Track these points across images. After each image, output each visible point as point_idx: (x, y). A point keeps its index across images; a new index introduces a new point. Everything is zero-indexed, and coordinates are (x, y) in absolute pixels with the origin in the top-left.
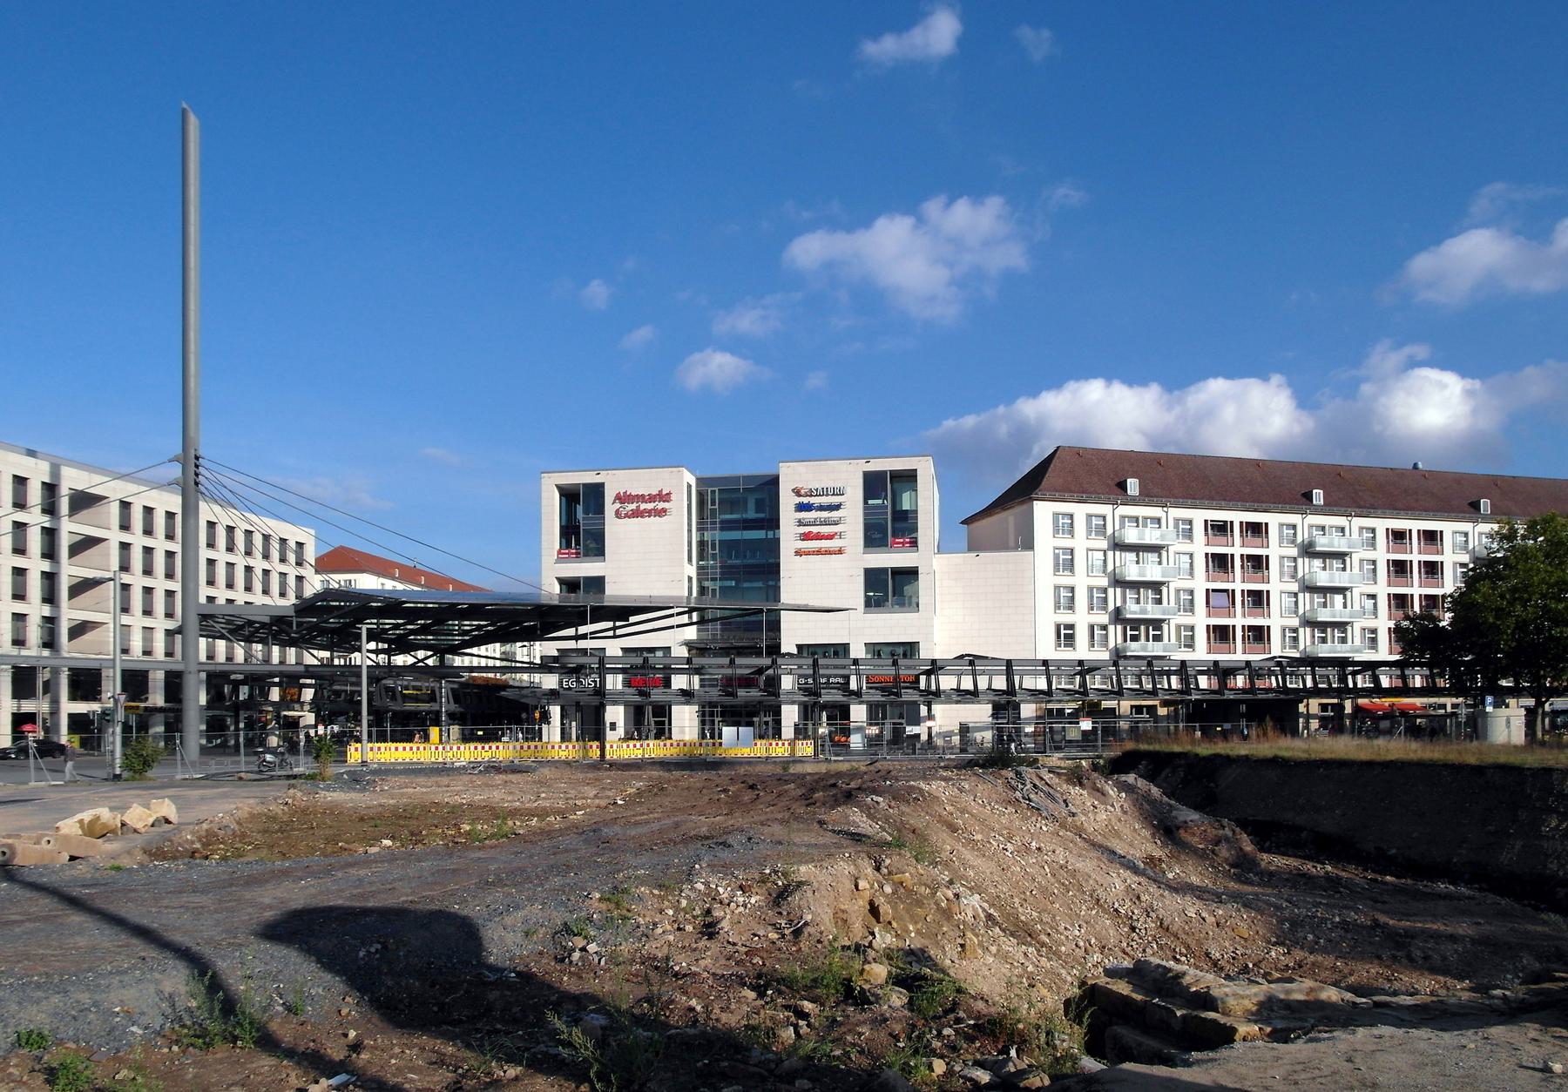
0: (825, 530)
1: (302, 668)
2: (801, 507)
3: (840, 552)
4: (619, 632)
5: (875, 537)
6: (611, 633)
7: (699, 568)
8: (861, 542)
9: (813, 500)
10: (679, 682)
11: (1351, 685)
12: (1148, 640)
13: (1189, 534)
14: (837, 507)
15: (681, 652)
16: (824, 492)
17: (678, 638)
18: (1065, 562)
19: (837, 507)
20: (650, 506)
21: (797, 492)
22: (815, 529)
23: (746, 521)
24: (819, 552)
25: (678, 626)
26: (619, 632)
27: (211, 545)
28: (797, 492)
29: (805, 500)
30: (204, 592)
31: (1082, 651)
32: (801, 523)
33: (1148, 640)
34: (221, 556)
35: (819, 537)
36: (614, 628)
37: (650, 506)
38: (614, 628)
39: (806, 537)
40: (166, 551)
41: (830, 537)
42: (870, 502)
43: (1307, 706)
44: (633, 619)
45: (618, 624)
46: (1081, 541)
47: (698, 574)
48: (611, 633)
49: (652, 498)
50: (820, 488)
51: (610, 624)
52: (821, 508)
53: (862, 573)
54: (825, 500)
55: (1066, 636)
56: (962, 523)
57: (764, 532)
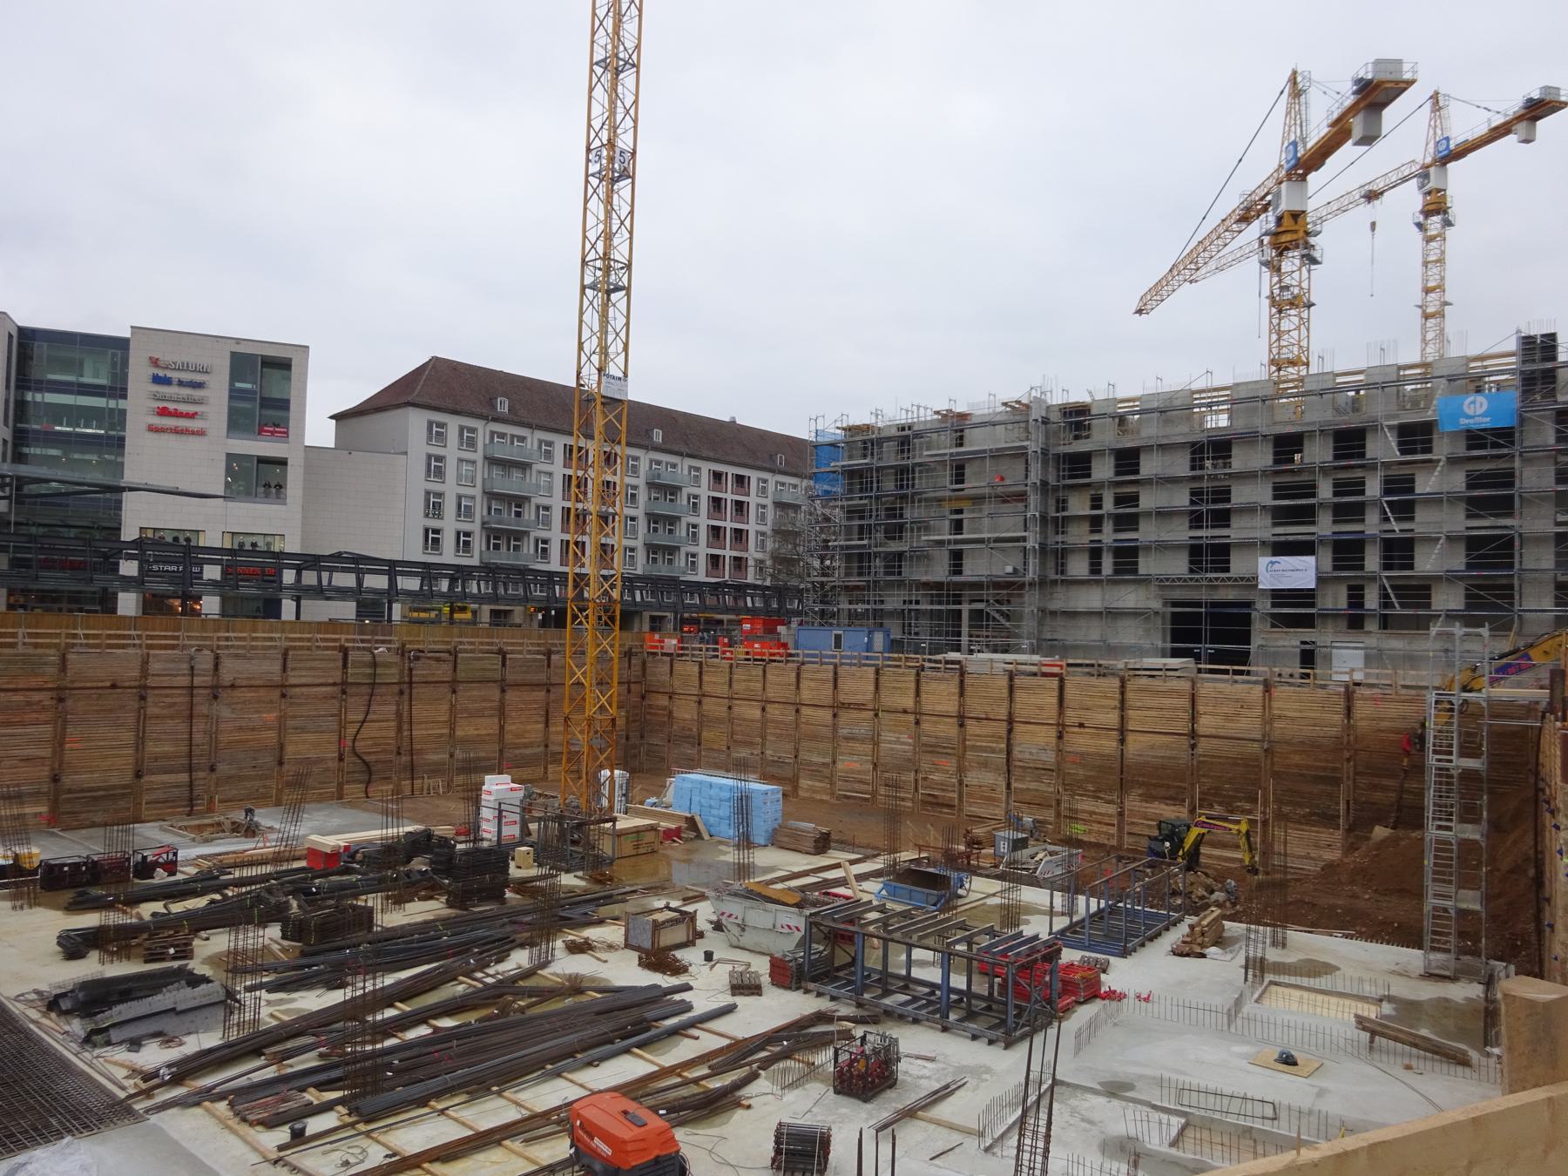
0: (183, 408)
2: (157, 380)
3: (201, 433)
5: (237, 423)
9: (175, 375)
11: (750, 604)
12: (509, 549)
13: (549, 455)
16: (184, 367)
18: (435, 467)
19: (199, 385)
22: (171, 406)
23: (81, 385)
24: (177, 431)
28: (155, 362)
29: (161, 373)
31: (448, 555)
32: (156, 398)
33: (509, 549)
39: (163, 412)
41: (192, 416)
42: (238, 385)
46: (452, 451)
47: (15, 438)
52: (181, 383)
54: (186, 376)
55: (432, 539)
56: (331, 417)
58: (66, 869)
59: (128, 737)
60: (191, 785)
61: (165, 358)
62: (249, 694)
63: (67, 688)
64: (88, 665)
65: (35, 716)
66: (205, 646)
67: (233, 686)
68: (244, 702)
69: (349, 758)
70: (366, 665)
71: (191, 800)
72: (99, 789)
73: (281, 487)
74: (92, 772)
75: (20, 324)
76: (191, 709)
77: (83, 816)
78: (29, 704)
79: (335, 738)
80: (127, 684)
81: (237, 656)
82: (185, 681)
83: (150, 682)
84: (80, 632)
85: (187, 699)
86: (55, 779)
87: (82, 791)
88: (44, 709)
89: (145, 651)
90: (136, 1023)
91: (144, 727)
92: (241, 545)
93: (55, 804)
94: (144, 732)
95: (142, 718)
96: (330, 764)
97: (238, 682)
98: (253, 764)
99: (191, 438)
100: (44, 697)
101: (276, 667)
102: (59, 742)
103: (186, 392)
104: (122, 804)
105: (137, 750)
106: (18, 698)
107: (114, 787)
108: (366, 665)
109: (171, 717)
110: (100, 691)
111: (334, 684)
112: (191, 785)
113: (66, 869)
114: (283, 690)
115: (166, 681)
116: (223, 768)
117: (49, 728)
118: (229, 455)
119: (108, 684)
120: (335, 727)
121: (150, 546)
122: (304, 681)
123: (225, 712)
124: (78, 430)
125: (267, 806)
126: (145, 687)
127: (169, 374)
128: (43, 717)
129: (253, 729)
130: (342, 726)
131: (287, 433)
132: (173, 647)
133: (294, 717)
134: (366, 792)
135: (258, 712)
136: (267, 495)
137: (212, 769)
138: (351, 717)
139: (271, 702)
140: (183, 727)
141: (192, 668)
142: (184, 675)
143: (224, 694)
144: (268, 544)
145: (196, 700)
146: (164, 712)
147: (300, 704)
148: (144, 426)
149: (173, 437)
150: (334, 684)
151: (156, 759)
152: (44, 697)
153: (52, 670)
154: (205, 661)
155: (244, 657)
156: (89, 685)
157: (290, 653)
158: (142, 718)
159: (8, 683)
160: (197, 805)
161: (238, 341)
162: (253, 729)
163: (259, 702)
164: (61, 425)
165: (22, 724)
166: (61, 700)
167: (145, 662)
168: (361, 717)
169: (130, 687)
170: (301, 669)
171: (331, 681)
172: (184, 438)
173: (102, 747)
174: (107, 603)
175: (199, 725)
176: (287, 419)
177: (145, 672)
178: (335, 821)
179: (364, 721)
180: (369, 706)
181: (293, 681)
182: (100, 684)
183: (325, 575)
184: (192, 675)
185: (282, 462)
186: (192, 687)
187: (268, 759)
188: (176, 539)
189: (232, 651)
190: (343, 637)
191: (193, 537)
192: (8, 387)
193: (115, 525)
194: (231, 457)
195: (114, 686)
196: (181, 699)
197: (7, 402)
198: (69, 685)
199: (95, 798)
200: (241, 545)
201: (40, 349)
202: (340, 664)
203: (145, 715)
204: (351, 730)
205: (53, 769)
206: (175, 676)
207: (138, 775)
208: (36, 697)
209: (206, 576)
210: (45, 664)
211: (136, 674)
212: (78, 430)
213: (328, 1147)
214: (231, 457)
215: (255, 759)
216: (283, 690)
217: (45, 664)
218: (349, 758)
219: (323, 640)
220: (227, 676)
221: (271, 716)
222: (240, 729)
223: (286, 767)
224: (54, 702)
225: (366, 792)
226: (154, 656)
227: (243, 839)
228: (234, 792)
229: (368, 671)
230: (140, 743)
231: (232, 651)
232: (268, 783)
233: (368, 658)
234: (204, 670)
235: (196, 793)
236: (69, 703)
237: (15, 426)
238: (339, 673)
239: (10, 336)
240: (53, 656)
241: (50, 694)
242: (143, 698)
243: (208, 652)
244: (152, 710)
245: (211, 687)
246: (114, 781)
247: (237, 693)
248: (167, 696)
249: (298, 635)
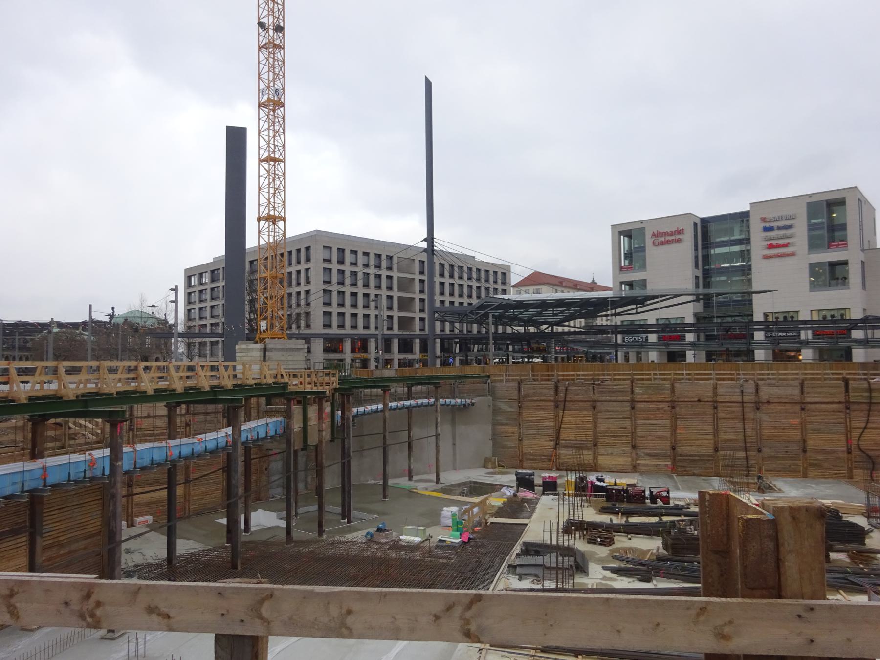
0: (781, 242)
1: (556, 288)
2: (766, 229)
3: (793, 254)
4: (639, 310)
5: (814, 245)
6: (634, 311)
7: (704, 270)
8: (806, 247)
10: (690, 337)
15: (690, 319)
17: (687, 313)
22: (774, 242)
25: (661, 308)
26: (639, 310)
27: (442, 275)
28: (764, 220)
29: (767, 225)
30: (438, 298)
34: (447, 280)
35: (779, 246)
36: (636, 308)
38: (636, 308)
39: (771, 247)
40: (338, 248)
41: (786, 246)
43: (575, 322)
44: (646, 303)
45: (638, 306)
47: (703, 274)
48: (634, 311)
49: (672, 234)
50: (777, 217)
51: (634, 306)
52: (779, 228)
53: (807, 266)
57: (716, 252)
58: (614, 491)
59: (710, 429)
60: (747, 458)
61: (770, 215)
62: (779, 407)
63: (675, 402)
64: (685, 389)
65: (661, 415)
66: (750, 379)
67: (768, 402)
68: (776, 413)
69: (856, 452)
70: (864, 390)
71: (748, 467)
72: (695, 456)
73: (846, 278)
74: (692, 446)
75: (702, 216)
76: (743, 415)
77: (688, 469)
78: (658, 409)
79: (843, 437)
80: (706, 400)
81: (769, 384)
82: (739, 399)
83: (720, 399)
84: (685, 372)
85: (741, 409)
86: (674, 448)
87: (687, 456)
88: (665, 412)
89: (715, 381)
90: (529, 567)
91: (717, 424)
92: (825, 317)
93: (674, 460)
94: (717, 427)
95: (716, 420)
96: (841, 455)
97: (771, 400)
98: (786, 449)
99: (787, 258)
100: (665, 406)
101: (797, 391)
102: (674, 429)
104: (708, 465)
105: (714, 436)
106: (652, 405)
107: (704, 455)
108: (864, 390)
109: (733, 419)
110: (692, 403)
111: (840, 403)
112: (747, 458)
113: (614, 491)
114: (803, 406)
115: (728, 399)
116: (766, 451)
117: (668, 422)
118: (811, 264)
119: (696, 400)
120: (843, 430)
121: (766, 325)
122: (816, 400)
123: (765, 418)
124: (732, 265)
125: (797, 477)
126: (716, 402)
127: (772, 224)
128: (665, 416)
129: (784, 429)
130: (848, 431)
131: (846, 244)
132: (732, 380)
133: (812, 423)
134: (871, 476)
135: (786, 418)
136: (837, 285)
137: (759, 451)
138: (854, 425)
139: (795, 413)
140: (740, 425)
141: (742, 392)
142: (738, 395)
143: (764, 407)
144: (842, 315)
145: (745, 410)
146: (728, 416)
147: (816, 415)
149: (777, 259)
150: (840, 403)
151: (725, 442)
152: (665, 406)
153: (668, 392)
154: (750, 388)
155: (774, 385)
156: (686, 400)
157: (806, 382)
158: (716, 420)
159: (648, 398)
160: (751, 471)
161: (810, 195)
162: (784, 429)
163: (786, 412)
164: (724, 264)
165: (656, 419)
166: (673, 407)
167: (715, 388)
168: (863, 425)
169: (708, 402)
170: (813, 392)
171: (836, 400)
172: (783, 259)
173: (696, 433)
174: (749, 355)
175: (749, 425)
176: (846, 236)
177: (715, 394)
178: (828, 492)
179: (865, 428)
180: (868, 418)
181: (808, 400)
182: (692, 400)
183: (869, 331)
184: (742, 395)
185: (845, 263)
186: (743, 402)
187: (795, 448)
188: (785, 318)
189: (768, 382)
190: (844, 372)
191: (795, 315)
192: (696, 249)
193: (750, 313)
194: (812, 266)
195: (699, 401)
196: (737, 409)
197: (696, 257)
198: (676, 400)
199: (694, 461)
200: (825, 317)
201: (712, 227)
202: (843, 389)
203: (717, 416)
204: (856, 434)
205: (672, 443)
206: (733, 396)
207: (716, 450)
208: (661, 405)
209: (688, 340)
210: (664, 389)
211: (710, 394)
212: (732, 265)
213: (506, 654)
214: (812, 266)
215: (787, 447)
216: (803, 406)
217: (664, 389)
218: (856, 452)
219: (660, 374)
220: (764, 396)
221: (796, 422)
222: (775, 428)
223: (808, 454)
224: (670, 408)
225: (871, 476)
226: (720, 385)
227: (757, 494)
228: (775, 466)
229: (867, 394)
230: (716, 432)
231: (768, 382)
232: (796, 462)
233: (864, 385)
234: (749, 393)
235: (750, 464)
236: (677, 409)
237: (703, 267)
238: (843, 395)
239: (695, 225)
240: (667, 385)
241: (667, 404)
242: (715, 408)
243: (753, 382)
244: (721, 415)
245: (755, 403)
246: (703, 452)
247: (772, 406)
248: (729, 407)
249: (729, 372)
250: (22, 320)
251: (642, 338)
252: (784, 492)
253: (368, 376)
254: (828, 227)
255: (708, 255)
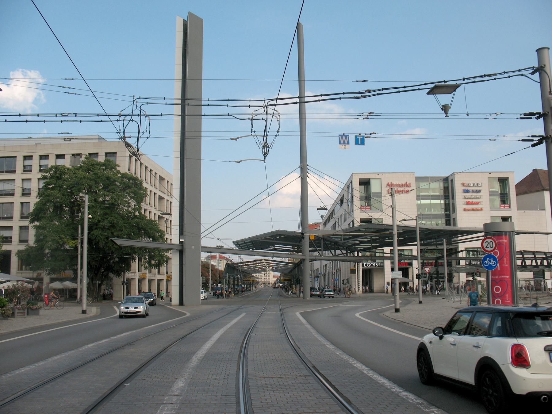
0: (475, 201)
2: (465, 191)
3: (481, 210)
14: (479, 191)
16: (474, 185)
19: (479, 191)
20: (402, 189)
21: (463, 185)
22: (471, 200)
24: (473, 210)
28: (463, 185)
29: (466, 188)
32: (465, 198)
37: (402, 189)
39: (468, 203)
49: (402, 186)
52: (473, 192)
54: (474, 189)
103: (474, 194)
148: (462, 210)
149: (473, 212)
250: (7, 249)
251: (379, 264)
252: (129, 154)
253: (513, 233)
254: (501, 194)
255: (445, 199)
